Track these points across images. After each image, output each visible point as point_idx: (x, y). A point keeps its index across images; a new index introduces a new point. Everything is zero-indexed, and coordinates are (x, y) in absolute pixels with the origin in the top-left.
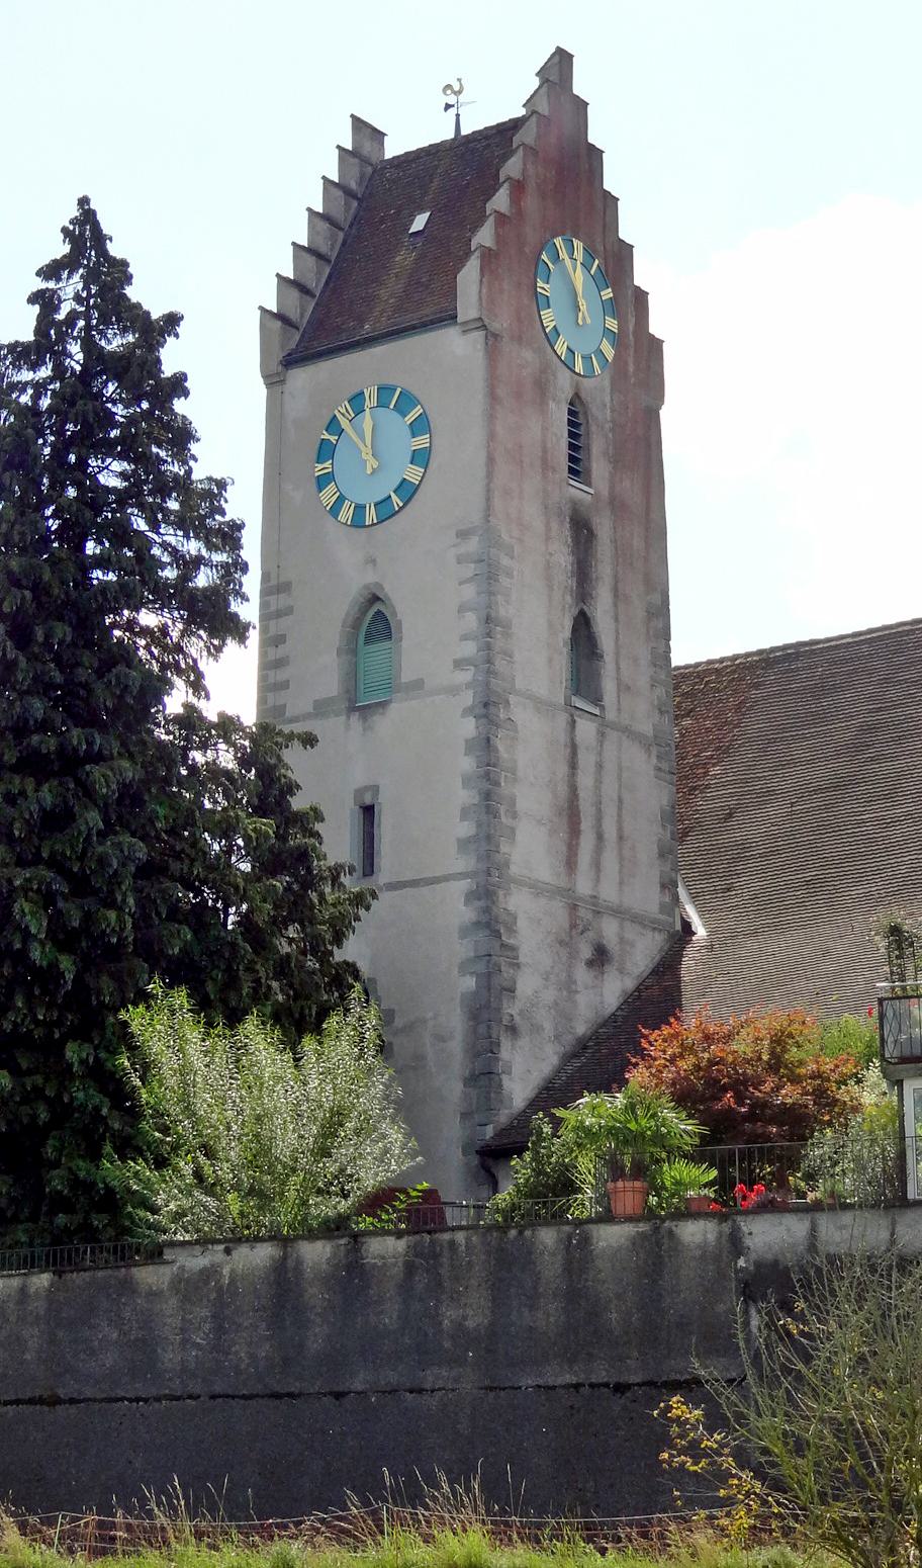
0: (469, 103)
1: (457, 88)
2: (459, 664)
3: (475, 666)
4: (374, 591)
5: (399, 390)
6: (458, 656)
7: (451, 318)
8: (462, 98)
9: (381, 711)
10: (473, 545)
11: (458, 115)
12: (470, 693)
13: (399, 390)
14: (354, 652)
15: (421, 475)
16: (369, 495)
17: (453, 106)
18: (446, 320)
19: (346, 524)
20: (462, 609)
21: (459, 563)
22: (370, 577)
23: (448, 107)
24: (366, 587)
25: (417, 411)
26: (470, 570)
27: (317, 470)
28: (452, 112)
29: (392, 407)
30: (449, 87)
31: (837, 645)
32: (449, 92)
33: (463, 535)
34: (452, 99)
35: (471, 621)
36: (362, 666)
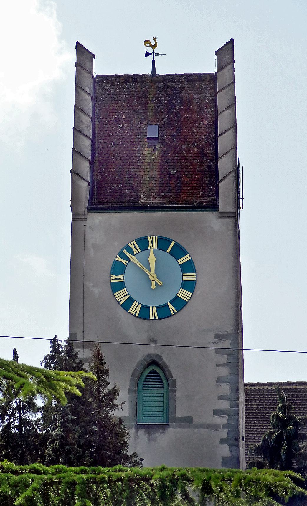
0: (160, 54)
1: (153, 43)
2: (216, 412)
3: (229, 416)
4: (155, 358)
5: (173, 243)
6: (217, 408)
7: (214, 207)
8: (156, 50)
9: (161, 431)
10: (227, 344)
11: (154, 61)
12: (226, 430)
13: (173, 243)
14: (137, 392)
15: (190, 296)
16: (154, 303)
17: (150, 54)
18: (211, 208)
19: (135, 315)
20: (219, 381)
21: (217, 354)
22: (152, 350)
23: (147, 54)
24: (149, 355)
25: (186, 258)
26: (224, 359)
27: (112, 278)
28: (150, 58)
29: (168, 251)
30: (147, 42)
31: (259, 389)
32: (148, 45)
33: (220, 337)
34: (150, 50)
35: (225, 389)
36: (141, 405)
